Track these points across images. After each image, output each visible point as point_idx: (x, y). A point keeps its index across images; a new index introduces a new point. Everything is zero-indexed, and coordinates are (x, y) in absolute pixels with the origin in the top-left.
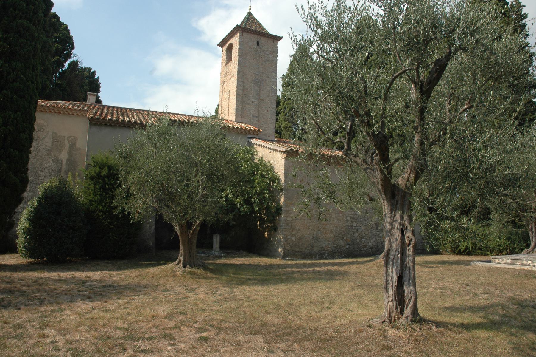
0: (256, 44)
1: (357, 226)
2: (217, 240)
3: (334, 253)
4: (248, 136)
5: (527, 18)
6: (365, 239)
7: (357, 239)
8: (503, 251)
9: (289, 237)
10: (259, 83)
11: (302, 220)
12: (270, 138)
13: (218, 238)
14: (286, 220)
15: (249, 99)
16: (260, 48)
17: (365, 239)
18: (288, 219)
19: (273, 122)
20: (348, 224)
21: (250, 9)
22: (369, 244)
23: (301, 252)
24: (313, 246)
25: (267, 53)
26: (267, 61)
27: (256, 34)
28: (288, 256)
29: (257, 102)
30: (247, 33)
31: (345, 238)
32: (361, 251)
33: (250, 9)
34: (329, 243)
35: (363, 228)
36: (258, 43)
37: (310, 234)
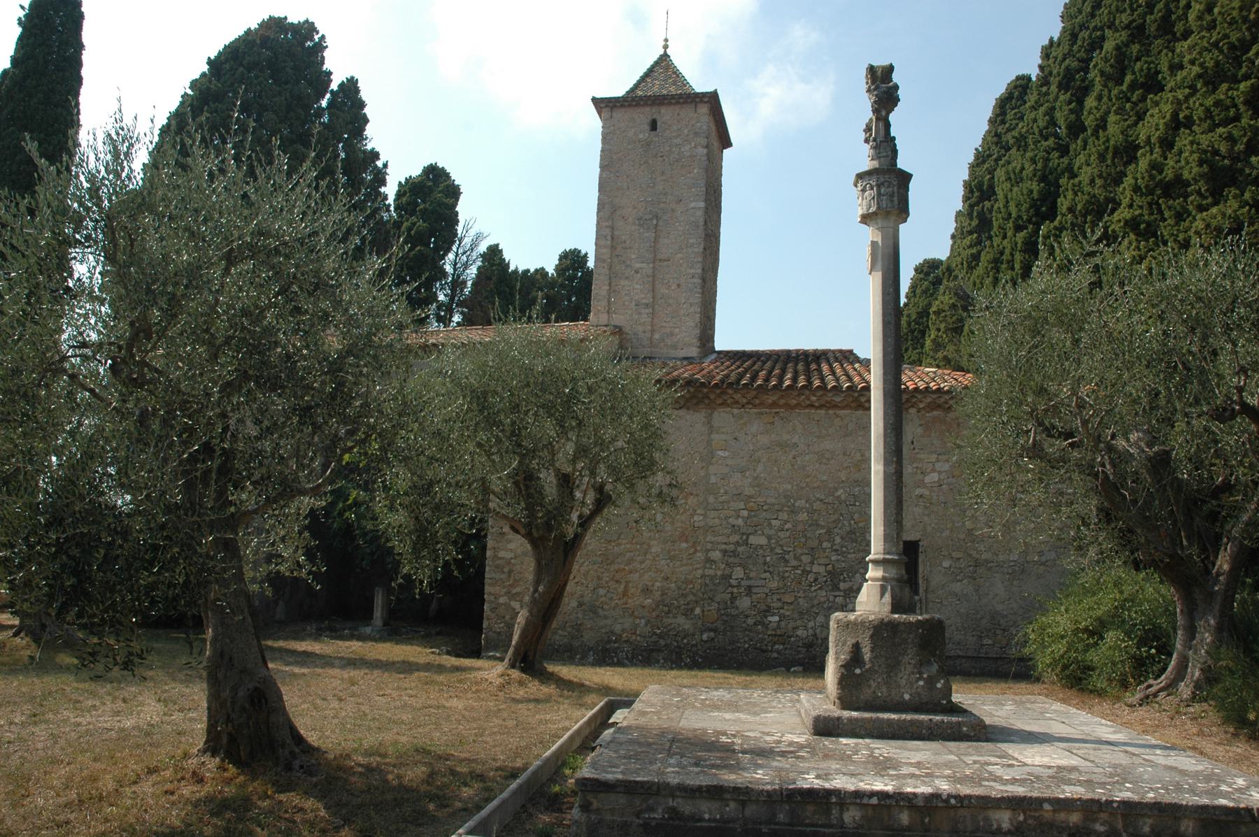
0: (647, 128)
1: (749, 578)
3: (652, 650)
7: (747, 617)
9: (502, 600)
10: (655, 222)
15: (627, 266)
16: (658, 136)
17: (782, 617)
18: (502, 554)
19: (692, 310)
20: (711, 572)
21: (666, 47)
22: (799, 633)
24: (578, 627)
25: (678, 141)
26: (677, 161)
27: (646, 104)
30: (624, 109)
31: (698, 611)
32: (764, 651)
33: (666, 47)
34: (637, 621)
35: (774, 585)
36: (654, 126)
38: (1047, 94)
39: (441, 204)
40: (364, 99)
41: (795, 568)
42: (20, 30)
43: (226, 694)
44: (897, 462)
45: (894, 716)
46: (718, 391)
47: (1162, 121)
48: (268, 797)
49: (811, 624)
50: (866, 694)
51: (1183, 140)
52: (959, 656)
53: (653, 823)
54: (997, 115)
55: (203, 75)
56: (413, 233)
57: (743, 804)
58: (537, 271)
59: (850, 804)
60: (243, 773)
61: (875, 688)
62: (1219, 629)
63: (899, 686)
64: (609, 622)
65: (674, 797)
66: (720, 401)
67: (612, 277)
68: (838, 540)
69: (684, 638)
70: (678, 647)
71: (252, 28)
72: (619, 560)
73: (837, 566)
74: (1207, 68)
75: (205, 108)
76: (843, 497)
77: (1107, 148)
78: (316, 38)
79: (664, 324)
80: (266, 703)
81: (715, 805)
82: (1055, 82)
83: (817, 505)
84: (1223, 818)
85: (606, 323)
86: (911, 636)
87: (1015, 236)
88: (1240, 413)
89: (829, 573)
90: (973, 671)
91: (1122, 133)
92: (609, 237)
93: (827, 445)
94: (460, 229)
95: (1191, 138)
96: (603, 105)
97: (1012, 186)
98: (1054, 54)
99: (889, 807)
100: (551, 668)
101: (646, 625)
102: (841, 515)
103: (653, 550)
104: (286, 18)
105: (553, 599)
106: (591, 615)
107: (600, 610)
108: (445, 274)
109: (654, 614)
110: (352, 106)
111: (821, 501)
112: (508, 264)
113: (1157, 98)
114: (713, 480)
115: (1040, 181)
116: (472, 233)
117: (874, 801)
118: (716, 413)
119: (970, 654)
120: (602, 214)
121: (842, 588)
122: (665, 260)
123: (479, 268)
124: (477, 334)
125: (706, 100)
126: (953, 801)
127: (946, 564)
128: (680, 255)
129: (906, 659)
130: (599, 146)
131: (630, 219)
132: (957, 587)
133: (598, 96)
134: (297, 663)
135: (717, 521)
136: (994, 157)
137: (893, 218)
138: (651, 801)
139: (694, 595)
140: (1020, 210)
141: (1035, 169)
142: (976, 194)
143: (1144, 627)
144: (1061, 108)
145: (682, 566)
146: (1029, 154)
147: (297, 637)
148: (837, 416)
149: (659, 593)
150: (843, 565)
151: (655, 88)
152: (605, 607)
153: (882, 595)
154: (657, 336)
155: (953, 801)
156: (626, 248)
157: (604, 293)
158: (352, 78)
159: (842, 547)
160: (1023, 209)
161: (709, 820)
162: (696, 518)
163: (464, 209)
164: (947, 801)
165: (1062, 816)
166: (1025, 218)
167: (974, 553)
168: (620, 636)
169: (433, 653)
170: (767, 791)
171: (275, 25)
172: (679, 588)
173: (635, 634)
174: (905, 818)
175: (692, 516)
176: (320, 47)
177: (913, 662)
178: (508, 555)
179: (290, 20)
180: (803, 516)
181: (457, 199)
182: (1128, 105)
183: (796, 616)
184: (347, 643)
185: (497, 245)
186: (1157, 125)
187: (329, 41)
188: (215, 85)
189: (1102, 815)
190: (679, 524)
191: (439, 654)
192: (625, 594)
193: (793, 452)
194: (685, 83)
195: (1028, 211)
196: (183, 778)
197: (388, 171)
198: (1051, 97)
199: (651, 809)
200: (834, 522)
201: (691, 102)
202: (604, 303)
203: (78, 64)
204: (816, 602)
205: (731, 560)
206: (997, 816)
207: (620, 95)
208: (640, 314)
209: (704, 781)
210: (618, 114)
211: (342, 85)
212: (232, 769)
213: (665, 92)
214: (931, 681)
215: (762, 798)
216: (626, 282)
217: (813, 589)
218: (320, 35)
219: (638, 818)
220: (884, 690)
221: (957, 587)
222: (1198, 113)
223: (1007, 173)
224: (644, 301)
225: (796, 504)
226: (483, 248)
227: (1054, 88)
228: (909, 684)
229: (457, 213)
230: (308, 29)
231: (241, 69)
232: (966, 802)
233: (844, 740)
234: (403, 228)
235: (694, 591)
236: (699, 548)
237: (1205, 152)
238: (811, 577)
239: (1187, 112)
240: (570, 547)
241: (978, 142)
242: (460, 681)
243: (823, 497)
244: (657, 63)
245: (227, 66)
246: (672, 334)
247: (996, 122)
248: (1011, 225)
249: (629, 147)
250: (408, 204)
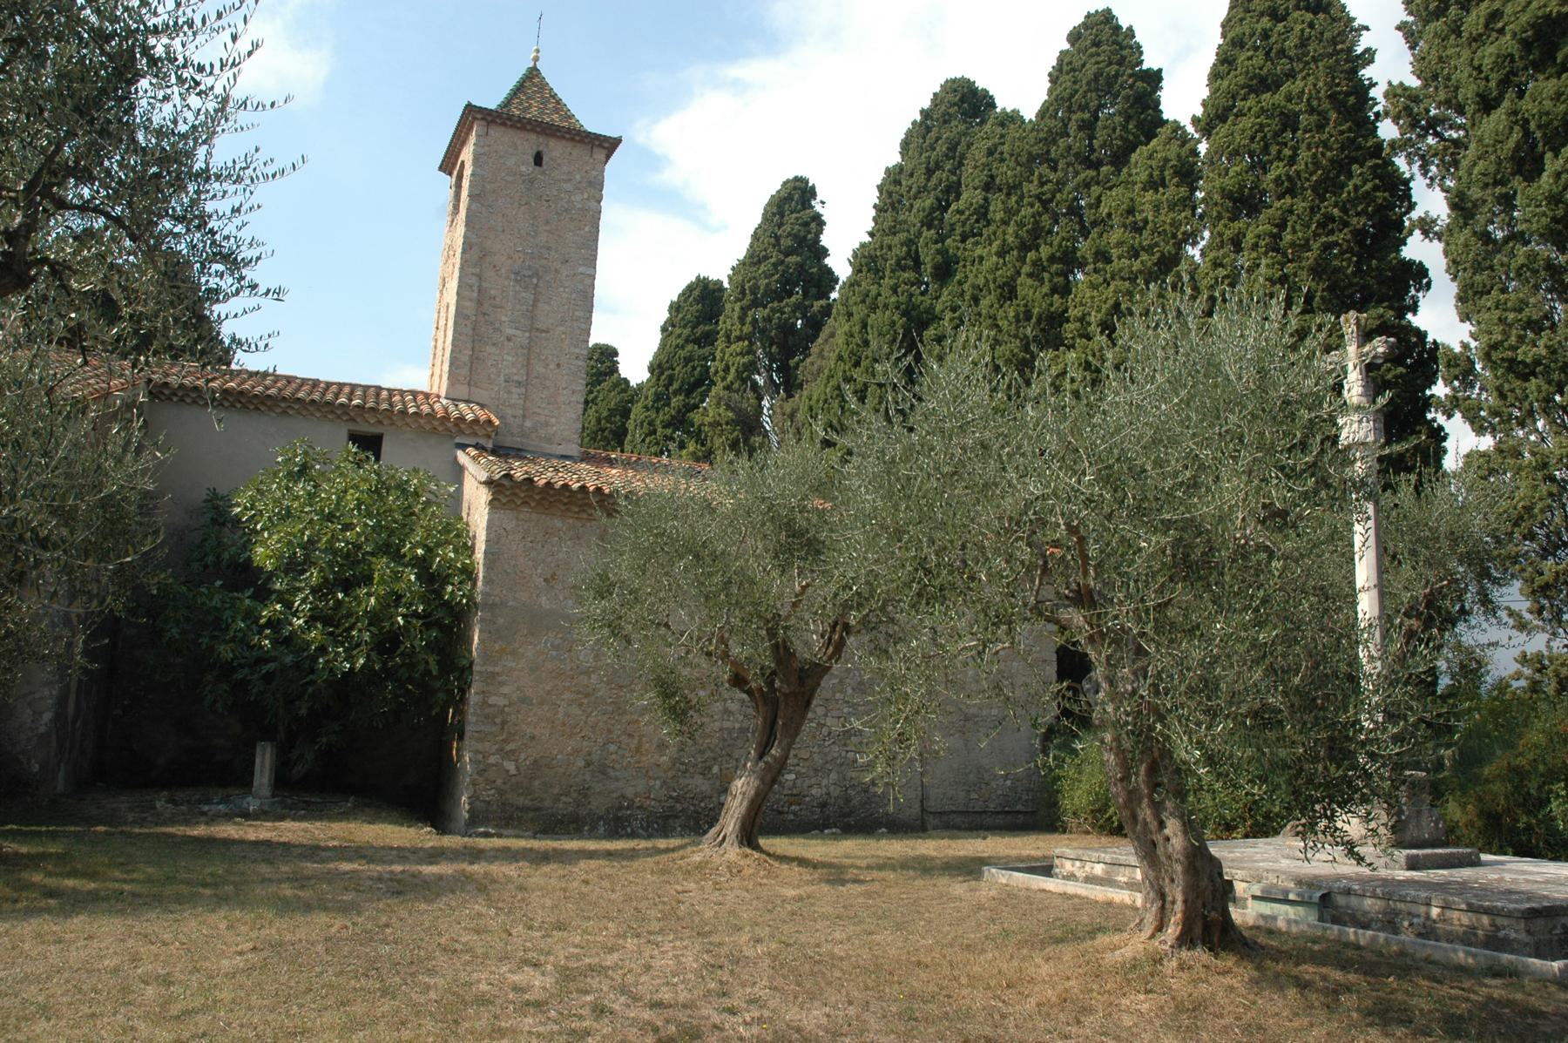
2: (262, 762)
3: (668, 817)
4: (458, 440)
5: (1371, 61)
6: (798, 774)
8: (1236, 827)
9: (492, 760)
10: (535, 281)
11: (546, 708)
12: (561, 450)
13: (268, 755)
14: (485, 704)
15: (496, 330)
16: (543, 173)
17: (798, 774)
18: (492, 700)
19: (574, 398)
20: (727, 724)
21: (536, 59)
22: (814, 791)
23: (537, 809)
24: (585, 792)
25: (568, 186)
26: (566, 210)
27: (533, 130)
28: (485, 821)
29: (522, 337)
30: (503, 129)
31: (715, 769)
32: (781, 813)
33: (536, 59)
34: (652, 783)
36: (538, 159)
37: (576, 751)
49: (825, 782)
50: (1409, 835)
61: (1412, 832)
68: (850, 691)
70: (695, 812)
79: (537, 410)
92: (475, 288)
96: (479, 116)
106: (601, 776)
107: (610, 770)
115: (903, 315)
119: (960, 808)
120: (467, 256)
128: (562, 328)
131: (503, 271)
136: (773, 260)
139: (712, 751)
152: (617, 766)
154: (528, 424)
156: (495, 306)
167: (963, 707)
173: (649, 797)
178: (501, 702)
183: (811, 773)
192: (638, 750)
204: (829, 758)
208: (510, 392)
224: (516, 378)
238: (825, 731)
246: (547, 424)
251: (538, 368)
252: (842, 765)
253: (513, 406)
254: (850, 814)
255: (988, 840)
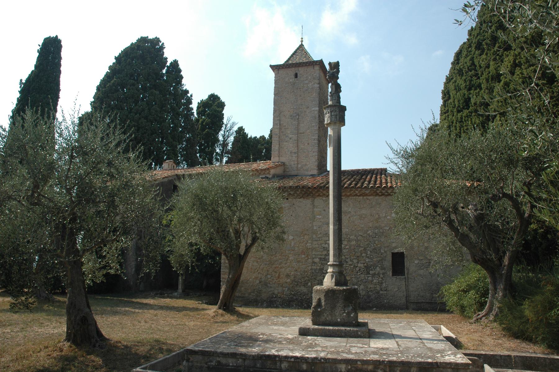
0: (293, 77)
15: (286, 136)
19: (314, 154)
20: (315, 267)
21: (302, 41)
25: (307, 82)
27: (292, 67)
30: (283, 69)
33: (302, 41)
34: (284, 289)
36: (296, 76)
37: (256, 278)
38: (470, 51)
39: (215, 111)
40: (181, 68)
41: (351, 265)
42: (38, 54)
43: (73, 318)
44: (338, 225)
45: (331, 328)
46: (316, 190)
47: (509, 64)
48: (83, 357)
50: (323, 319)
51: (518, 71)
52: (422, 302)
53: (211, 367)
54: (455, 60)
55: (114, 63)
56: (204, 123)
57: (244, 360)
58: (261, 137)
59: (284, 361)
60: (77, 348)
61: (325, 316)
62: (505, 289)
63: (336, 316)
64: (272, 289)
65: (219, 357)
66: (317, 194)
67: (280, 142)
68: (369, 252)
69: (304, 296)
71: (134, 42)
72: (276, 263)
73: (369, 264)
74: (528, 39)
75: (115, 77)
76: (371, 234)
77: (489, 77)
78: (160, 44)
80: (87, 321)
81: (234, 360)
82: (474, 46)
83: (360, 238)
84: (427, 366)
85: (278, 161)
86: (341, 295)
87: (457, 115)
88: (503, 197)
89: (365, 267)
90: (429, 309)
91: (495, 69)
92: (278, 125)
93: (364, 212)
94: (225, 121)
95: (520, 71)
96: (274, 68)
97: (457, 92)
98: (473, 33)
99: (299, 362)
100: (238, 309)
101: (288, 290)
102: (370, 242)
103: (290, 259)
104: (148, 37)
105: (236, 280)
107: (268, 284)
108: (218, 140)
109: (291, 286)
110: (176, 72)
111: (361, 236)
112: (247, 135)
113: (508, 53)
114: (315, 228)
116: (231, 122)
117: (293, 360)
118: (316, 199)
119: (427, 301)
120: (275, 114)
121: (371, 273)
122: (302, 133)
123: (234, 137)
124: (233, 167)
125: (318, 63)
126: (322, 360)
127: (416, 262)
128: (308, 131)
129: (339, 305)
130: (273, 85)
132: (421, 272)
133: (273, 64)
134: (140, 308)
135: (317, 245)
137: (337, 125)
138: (211, 358)
139: (308, 277)
140: (459, 103)
141: (466, 85)
142: (447, 96)
143: (483, 289)
144: (477, 57)
145: (302, 265)
146: (464, 78)
147: (146, 297)
148: (368, 199)
149: (293, 277)
150: (371, 263)
151: (297, 60)
152: (271, 283)
153: (332, 279)
154: (299, 166)
155: (322, 360)
156: (285, 129)
157: (277, 148)
158: (176, 60)
159: (371, 255)
160: (461, 102)
161: (232, 366)
162: (308, 244)
163: (226, 112)
164: (320, 360)
165: (365, 367)
166: (461, 107)
168: (277, 295)
169: (198, 303)
170: (253, 355)
171: (143, 40)
172: (301, 274)
173: (283, 294)
174: (304, 367)
175: (306, 244)
176: (162, 48)
177: (341, 306)
179: (149, 38)
180: (354, 243)
181: (223, 109)
182: (498, 57)
184: (165, 300)
185: (242, 127)
186: (507, 65)
187: (165, 45)
188: (118, 67)
189: (381, 366)
190: (301, 247)
191: (201, 304)
192: (279, 277)
193: (349, 215)
194: (309, 57)
195: (463, 103)
196: (55, 350)
197: (193, 98)
198: (472, 53)
199: (211, 361)
200: (367, 245)
201: (312, 65)
202: (277, 153)
203: (60, 65)
204: (360, 279)
205: (323, 262)
206: (340, 367)
207: (282, 63)
208: (292, 156)
209: (232, 351)
210: (281, 71)
211: (171, 63)
212: (74, 347)
213: (301, 61)
214: (349, 314)
215: (251, 358)
216: (286, 143)
217: (358, 274)
218: (162, 43)
219: (206, 364)
220: (330, 317)
221: (421, 272)
222: (523, 60)
223: (455, 86)
224: (294, 151)
225: (351, 238)
226: (235, 128)
227: (473, 48)
228: (340, 314)
229: (223, 114)
230: (156, 41)
231: (129, 60)
232: (328, 361)
233: (309, 337)
234: (200, 122)
235: (308, 276)
236: (309, 257)
237: (526, 78)
238: (357, 269)
239: (519, 60)
240: (241, 259)
241: (447, 73)
242: (198, 315)
243: (362, 234)
244: (298, 49)
245: (123, 59)
246: (306, 165)
247: (454, 63)
248: (455, 110)
249: (286, 85)
250: (202, 111)
251: (301, 146)
252: (366, 282)
253: (294, 161)
254: (369, 302)
255: (404, 315)
